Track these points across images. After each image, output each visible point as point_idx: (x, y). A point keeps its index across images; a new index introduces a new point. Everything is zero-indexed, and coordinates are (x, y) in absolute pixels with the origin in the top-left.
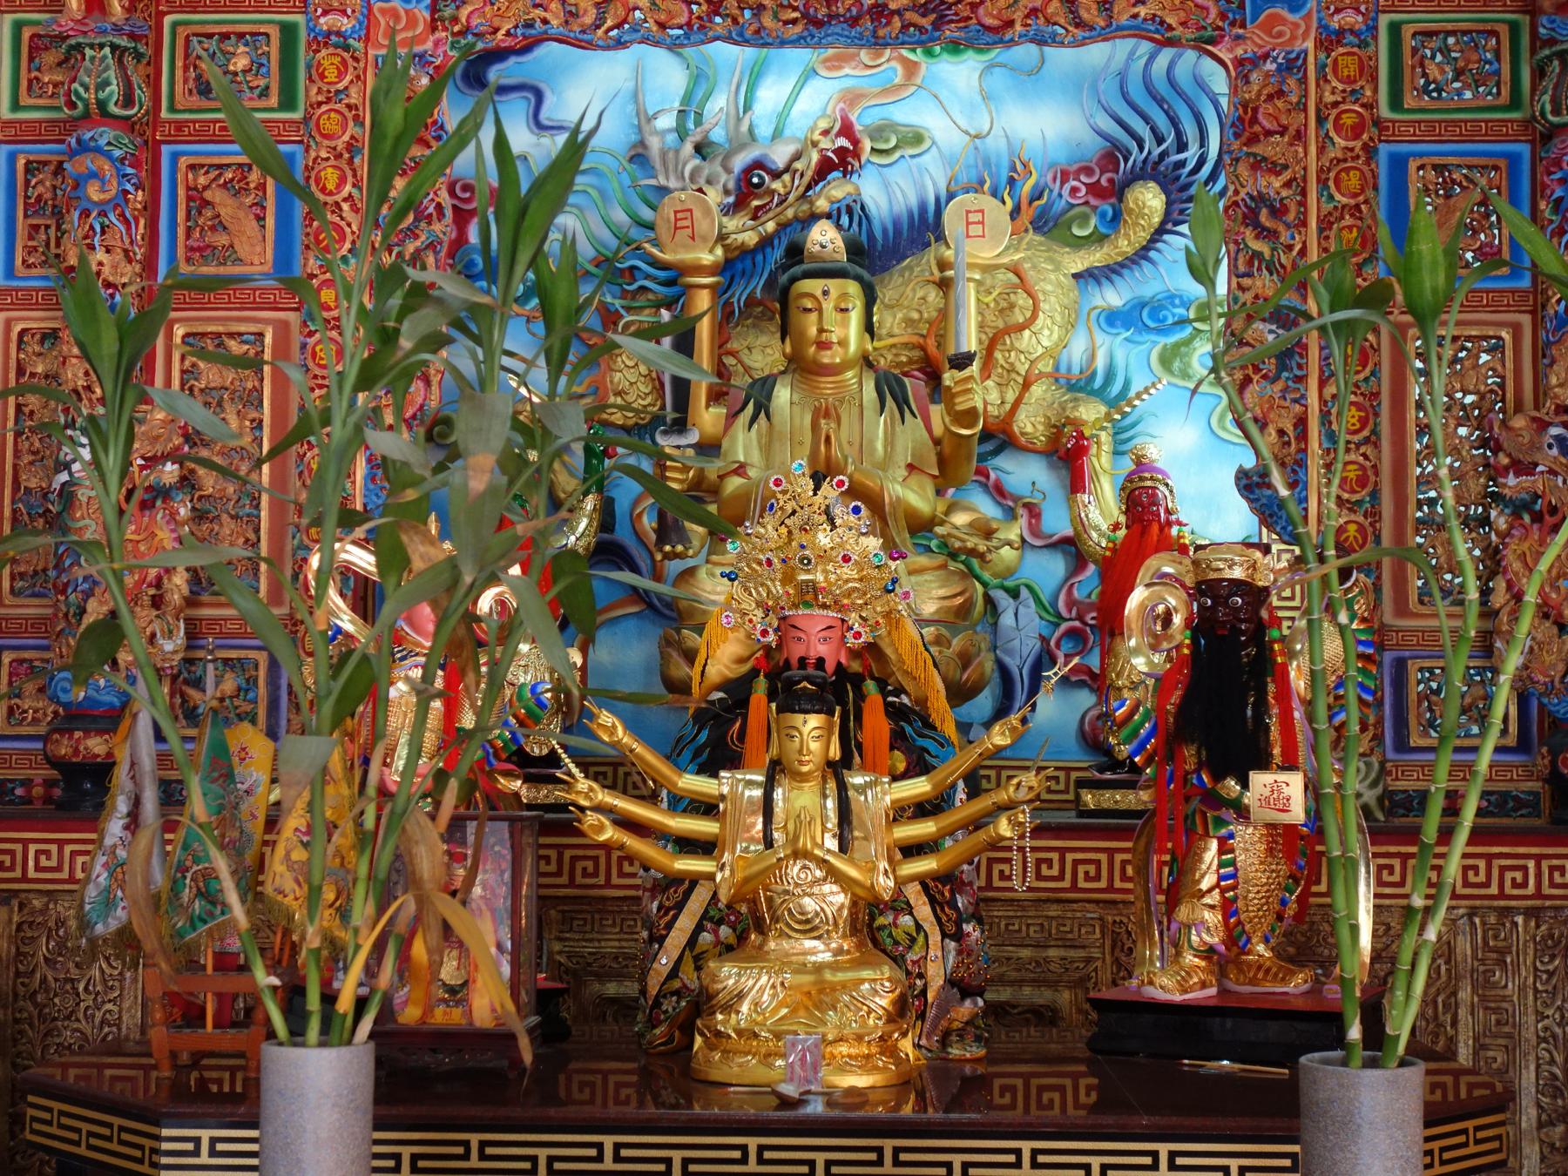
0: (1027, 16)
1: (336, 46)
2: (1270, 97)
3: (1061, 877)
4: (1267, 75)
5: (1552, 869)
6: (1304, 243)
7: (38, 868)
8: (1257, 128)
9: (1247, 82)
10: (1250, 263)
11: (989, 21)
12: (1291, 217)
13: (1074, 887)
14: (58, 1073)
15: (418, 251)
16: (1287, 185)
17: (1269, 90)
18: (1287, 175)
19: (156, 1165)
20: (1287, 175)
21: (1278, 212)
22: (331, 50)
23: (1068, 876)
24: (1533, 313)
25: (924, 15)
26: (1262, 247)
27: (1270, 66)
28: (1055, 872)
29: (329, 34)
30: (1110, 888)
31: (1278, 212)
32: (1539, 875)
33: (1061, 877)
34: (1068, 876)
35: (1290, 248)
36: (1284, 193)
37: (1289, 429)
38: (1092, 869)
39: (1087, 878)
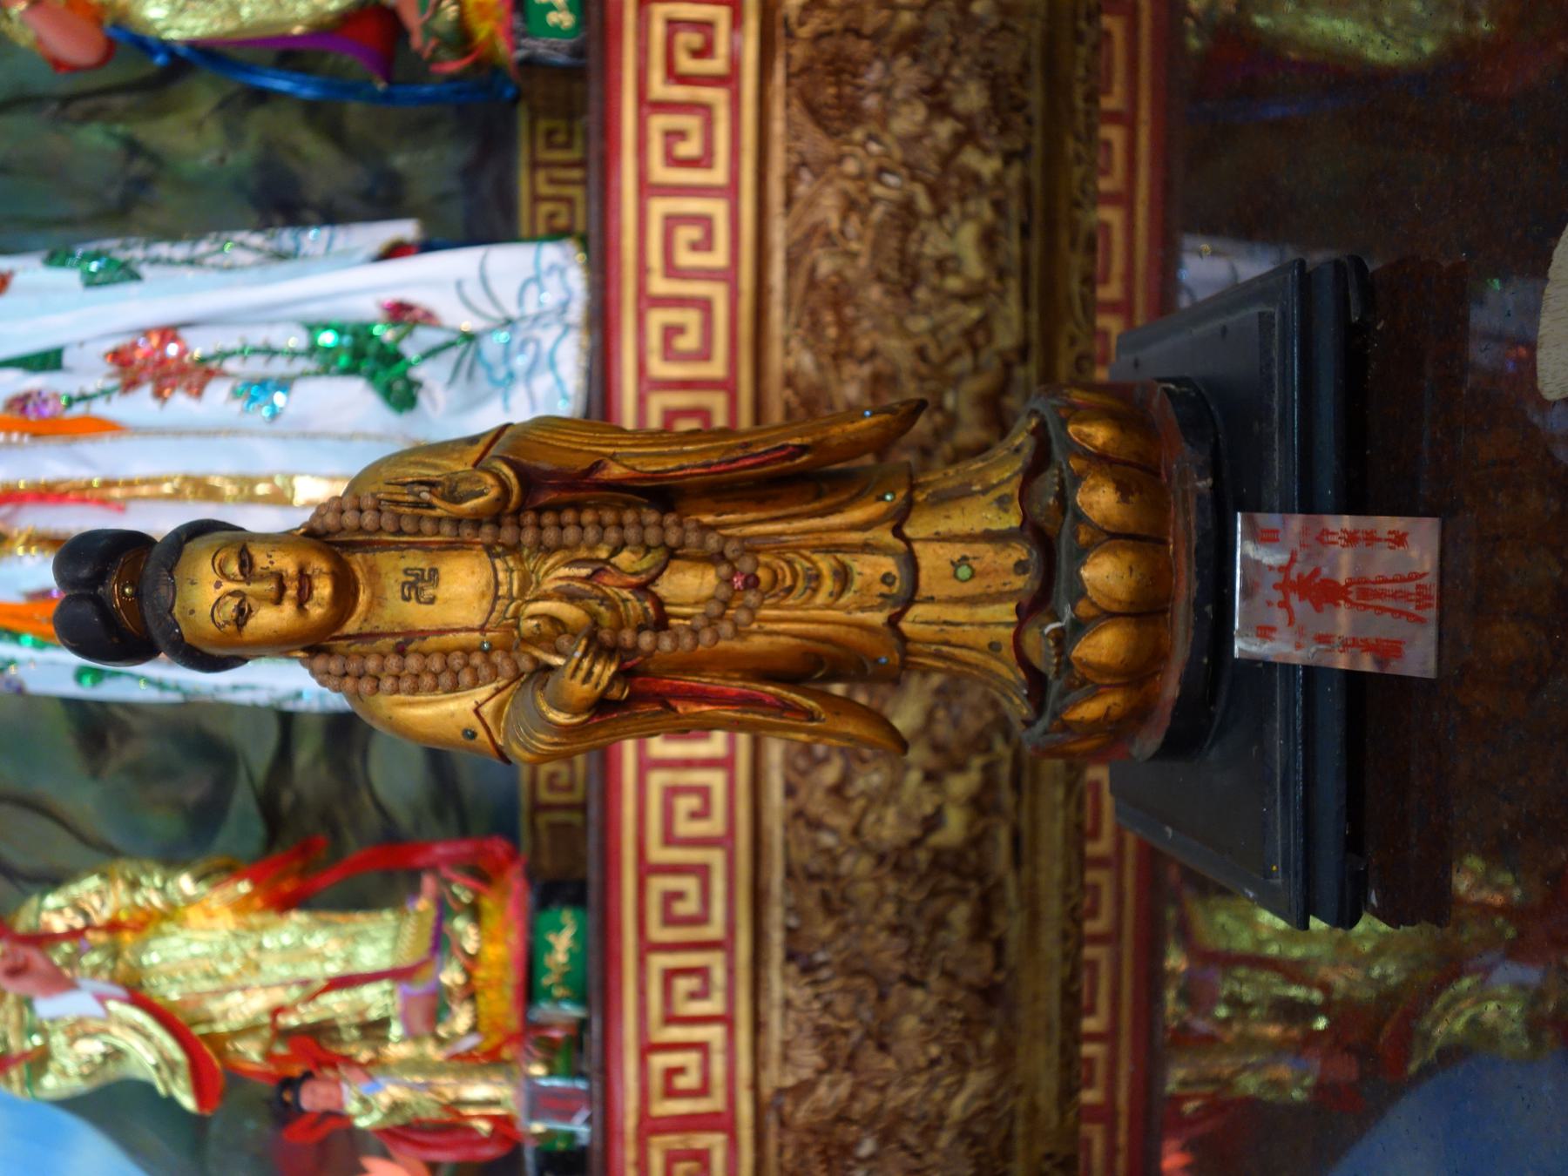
32: (689, 764)
38: (686, 234)
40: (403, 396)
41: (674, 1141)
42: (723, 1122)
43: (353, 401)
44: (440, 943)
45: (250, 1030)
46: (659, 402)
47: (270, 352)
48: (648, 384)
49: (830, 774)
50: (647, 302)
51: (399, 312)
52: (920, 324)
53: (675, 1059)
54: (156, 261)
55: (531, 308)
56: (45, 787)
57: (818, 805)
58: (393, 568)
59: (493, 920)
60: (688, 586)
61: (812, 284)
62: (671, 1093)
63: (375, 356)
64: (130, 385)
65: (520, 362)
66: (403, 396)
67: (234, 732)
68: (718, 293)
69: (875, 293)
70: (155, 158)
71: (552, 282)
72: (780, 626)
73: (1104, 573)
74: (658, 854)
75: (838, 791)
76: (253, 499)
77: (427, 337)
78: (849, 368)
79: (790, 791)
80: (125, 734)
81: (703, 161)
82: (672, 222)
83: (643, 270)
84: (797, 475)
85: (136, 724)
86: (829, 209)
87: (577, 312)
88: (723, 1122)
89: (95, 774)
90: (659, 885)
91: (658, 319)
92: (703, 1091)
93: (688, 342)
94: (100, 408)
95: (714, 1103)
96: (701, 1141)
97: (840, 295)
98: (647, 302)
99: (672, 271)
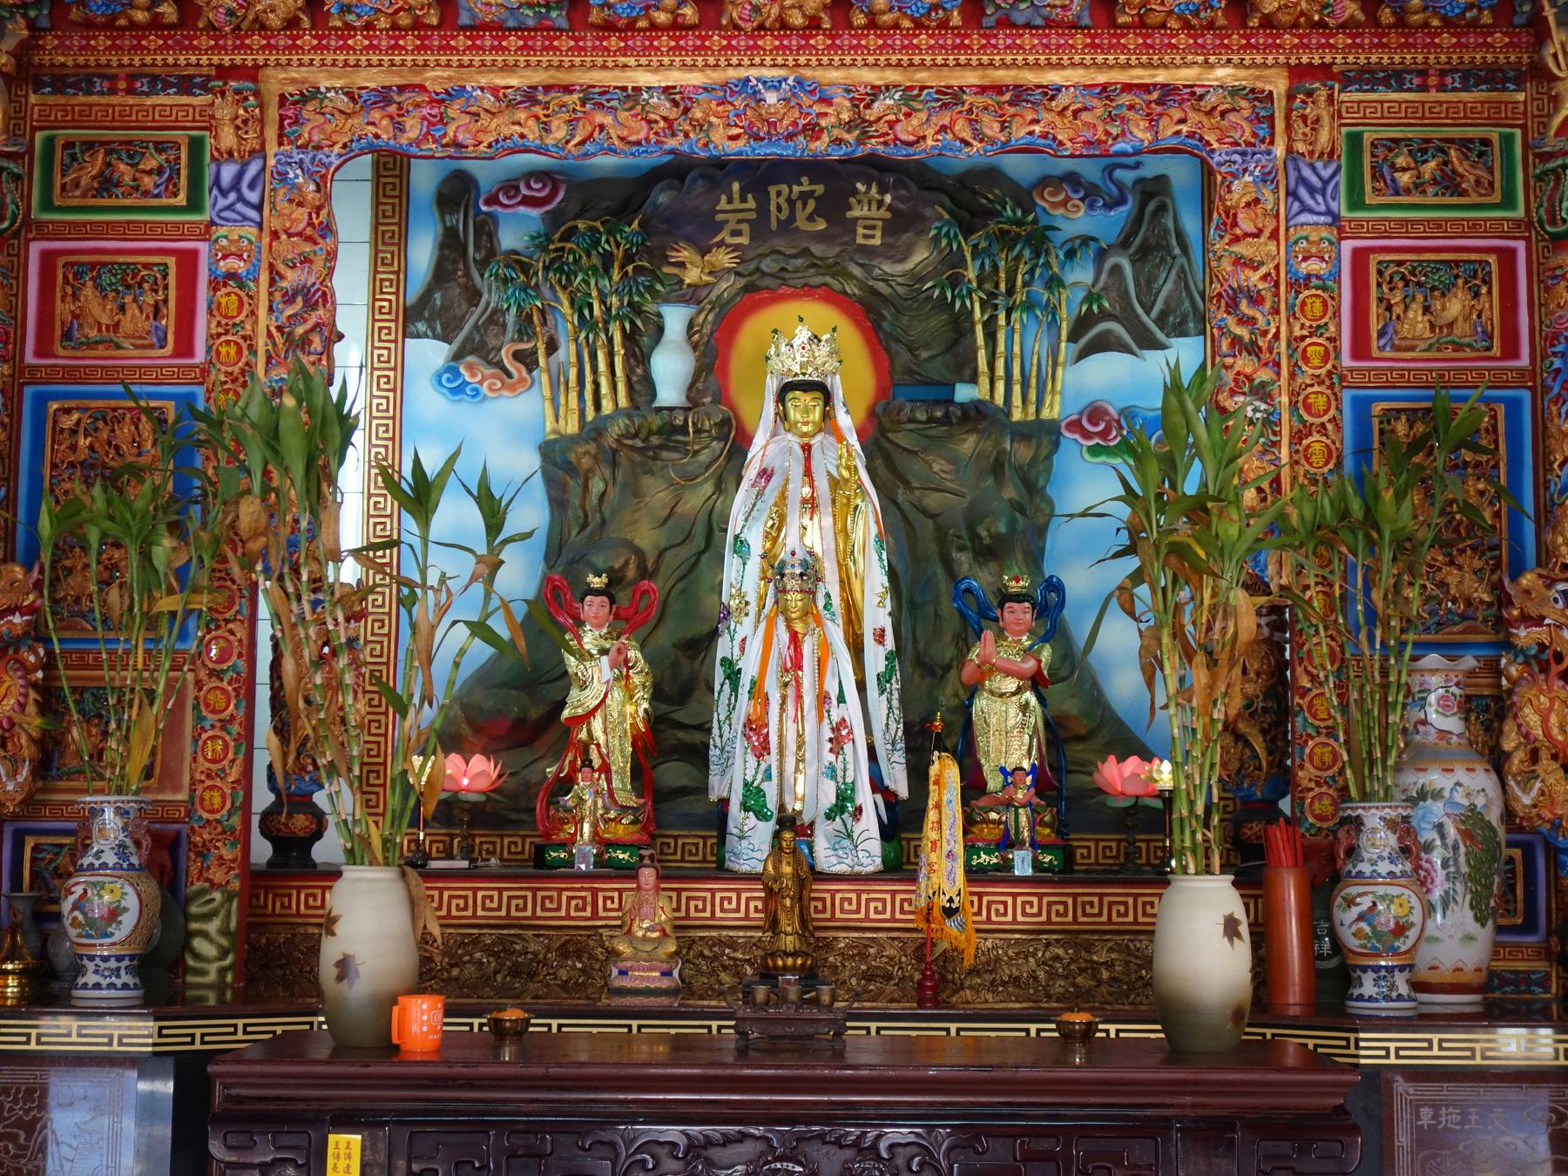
0: (938, 133)
1: (1317, 288)
2: (1248, 205)
3: (858, 911)
4: (1246, 185)
5: (1145, 904)
6: (1278, 328)
7: (525, 898)
8: (1238, 231)
9: (1230, 191)
10: (1232, 345)
11: (904, 137)
12: (1268, 305)
13: (1110, 921)
14: (90, 1092)
15: (307, 332)
16: (1265, 278)
17: (1248, 198)
18: (1263, 270)
19: (710, 1163)
20: (1263, 270)
21: (1256, 300)
22: (1313, 292)
23: (683, 907)
24: (1533, 389)
25: (849, 131)
26: (1243, 332)
27: (1248, 178)
28: (495, 905)
29: (1309, 276)
30: (1136, 922)
31: (1256, 300)
32: (713, 905)
33: (738, 910)
34: (683, 907)
35: (1265, 333)
36: (1260, 286)
37: (1265, 485)
38: (880, 905)
39: (1119, 914)
40: (830, 816)
41: (589, 899)
42: (595, 915)
43: (829, 797)
44: (624, 809)
45: (589, 732)
46: (1143, 845)
47: (845, 770)
48: (833, 893)
49: (706, 952)
50: (859, 893)
51: (859, 810)
52: (854, 981)
53: (496, 898)
54: (889, 701)
55: (861, 854)
56: (669, 622)
57: (697, 948)
58: (791, 860)
59: (633, 828)
60: (788, 902)
61: (866, 946)
62: (605, 899)
63: (843, 804)
64: (833, 729)
65: (840, 853)
66: (830, 816)
67: (693, 706)
68: (862, 915)
69: (864, 967)
70: (943, 677)
71: (869, 861)
72: (782, 916)
73: (790, 961)
74: (684, 895)
75: (701, 955)
76: (798, 761)
77: (849, 821)
78: (839, 959)
79: (702, 938)
80: (692, 658)
81: (902, 911)
82: (884, 901)
83: (869, 892)
84: (804, 922)
85: (697, 663)
86: (890, 952)
87: (857, 869)
88: (595, 915)
89: (675, 646)
90: (734, 896)
91: (854, 896)
92: (605, 909)
93: (846, 906)
94: (826, 721)
95: (601, 913)
96: (589, 908)
97: (863, 956)
98: (859, 893)
99: (868, 901)
